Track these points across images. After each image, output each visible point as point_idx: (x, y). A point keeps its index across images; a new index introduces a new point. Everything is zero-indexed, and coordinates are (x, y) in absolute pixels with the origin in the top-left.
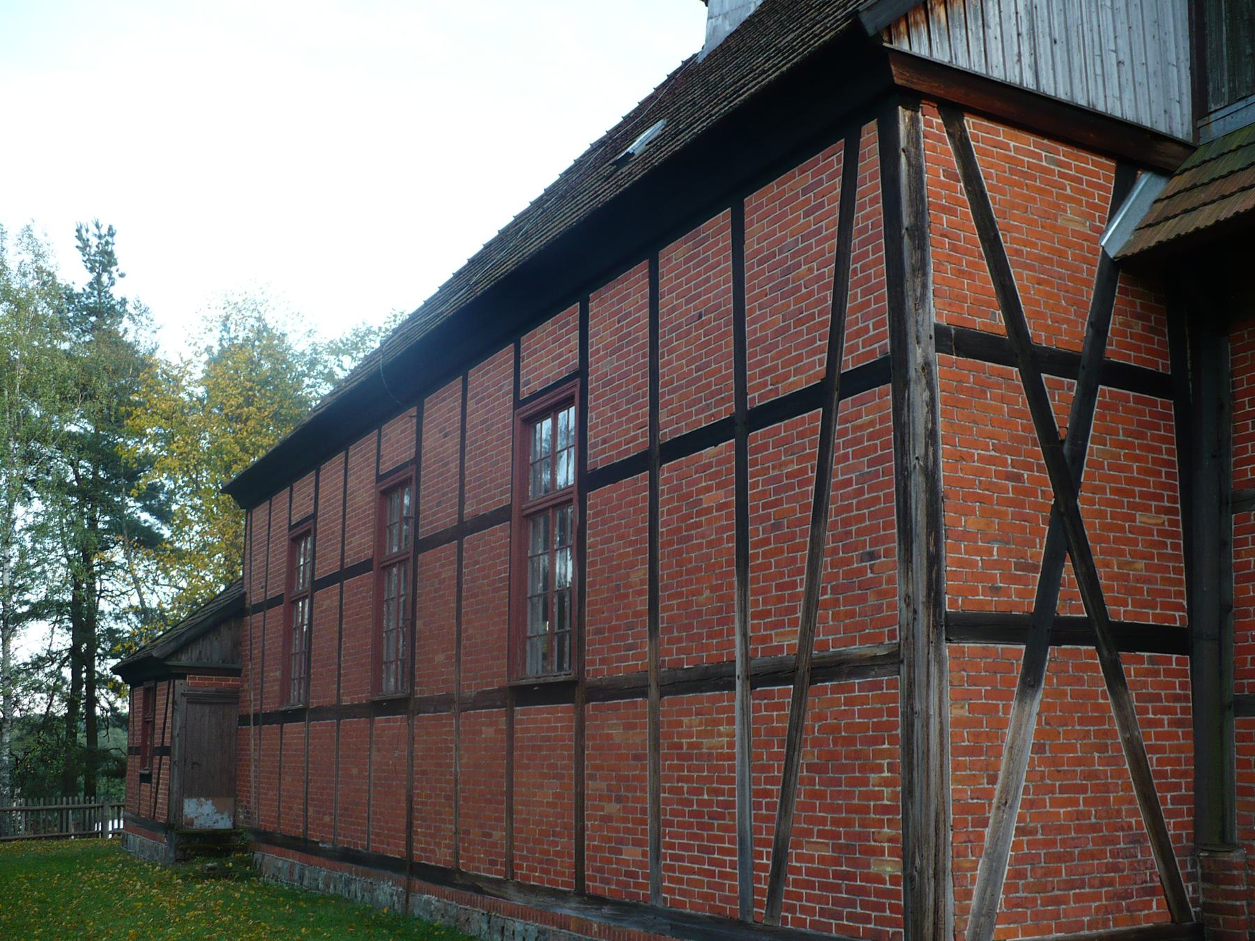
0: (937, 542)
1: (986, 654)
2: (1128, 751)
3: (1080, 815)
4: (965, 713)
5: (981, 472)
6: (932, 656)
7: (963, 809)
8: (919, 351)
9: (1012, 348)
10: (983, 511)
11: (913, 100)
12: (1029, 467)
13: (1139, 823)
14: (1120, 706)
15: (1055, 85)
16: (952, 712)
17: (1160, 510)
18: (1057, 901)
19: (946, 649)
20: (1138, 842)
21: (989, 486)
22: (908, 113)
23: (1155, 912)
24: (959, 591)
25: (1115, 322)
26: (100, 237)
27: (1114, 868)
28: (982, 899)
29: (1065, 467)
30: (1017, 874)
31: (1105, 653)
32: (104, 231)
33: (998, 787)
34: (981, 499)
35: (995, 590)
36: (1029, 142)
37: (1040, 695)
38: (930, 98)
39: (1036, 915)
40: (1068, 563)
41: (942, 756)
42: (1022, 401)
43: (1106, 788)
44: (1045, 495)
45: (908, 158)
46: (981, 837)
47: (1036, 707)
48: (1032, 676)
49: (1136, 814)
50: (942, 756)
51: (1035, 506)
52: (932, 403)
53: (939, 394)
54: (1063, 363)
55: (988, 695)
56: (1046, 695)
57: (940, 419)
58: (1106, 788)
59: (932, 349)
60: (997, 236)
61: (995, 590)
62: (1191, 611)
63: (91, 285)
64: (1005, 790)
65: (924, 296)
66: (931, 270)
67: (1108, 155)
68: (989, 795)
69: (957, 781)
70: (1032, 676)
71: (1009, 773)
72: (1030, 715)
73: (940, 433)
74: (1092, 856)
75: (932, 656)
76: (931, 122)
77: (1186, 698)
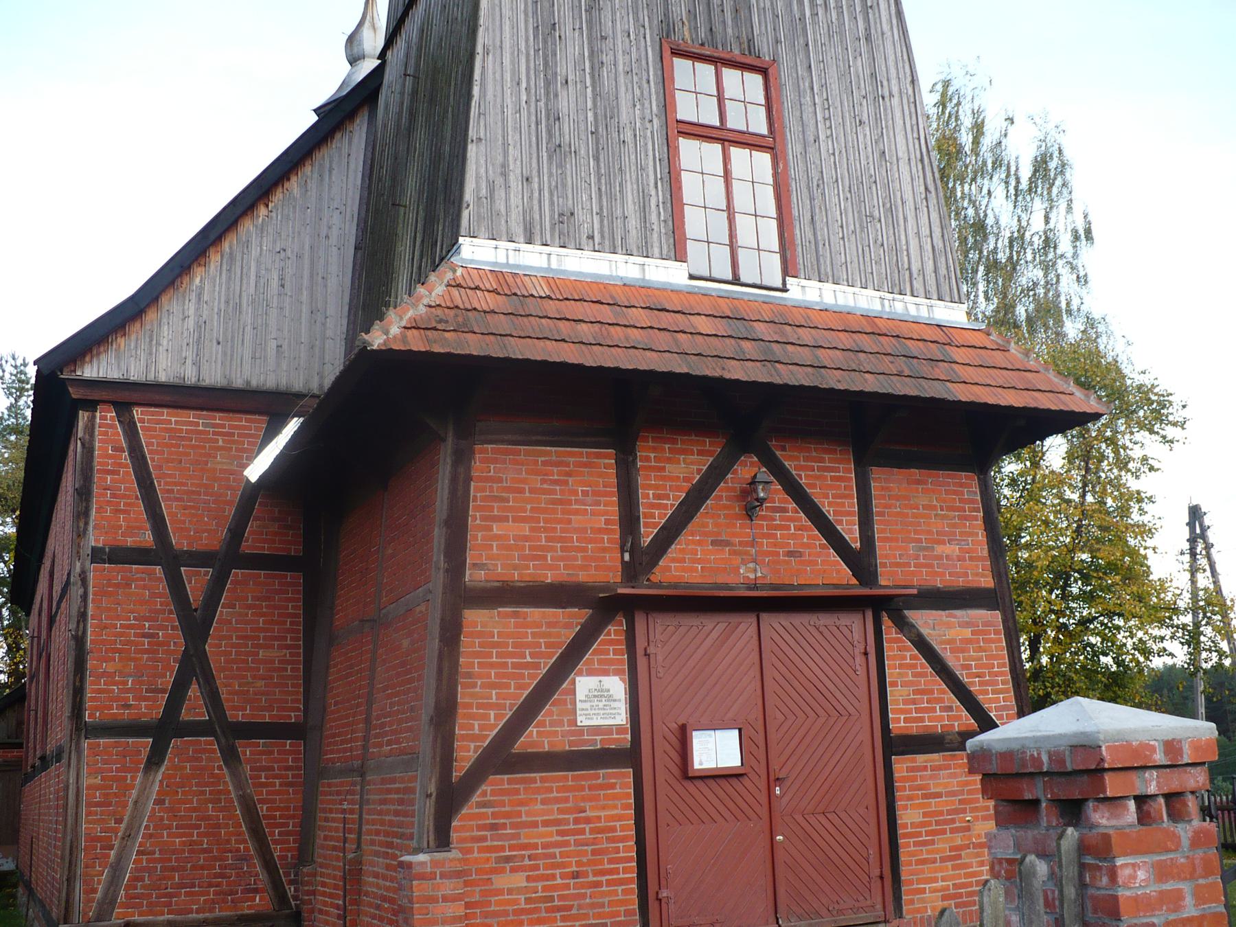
0: (82, 680)
1: (117, 745)
2: (240, 803)
3: (191, 843)
4: (98, 781)
5: (121, 634)
6: (73, 748)
7: (93, 839)
8: (78, 564)
9: (163, 554)
10: (121, 659)
11: (91, 405)
12: (164, 628)
13: (247, 849)
14: (235, 774)
15: (213, 376)
16: (86, 782)
17: (281, 647)
18: (170, 896)
19: (85, 744)
20: (245, 859)
21: (128, 643)
22: (86, 414)
23: (260, 902)
24: (97, 708)
25: (252, 526)
26: (16, 367)
27: (222, 876)
28: (106, 894)
29: (196, 625)
30: (135, 879)
31: (223, 741)
32: (19, 362)
33: (123, 826)
34: (119, 651)
35: (127, 706)
36: (191, 416)
37: (163, 769)
38: (104, 402)
39: (150, 904)
40: (194, 686)
41: (77, 807)
42: (163, 587)
43: (218, 826)
44: (178, 643)
45: (83, 444)
46: (108, 856)
47: (159, 777)
48: (155, 760)
49: (245, 841)
50: (77, 807)
51: (167, 652)
52: (85, 597)
53: (91, 590)
54: (199, 559)
55: (118, 770)
56: (167, 769)
57: (91, 605)
58: (218, 826)
59: (88, 562)
60: (152, 483)
61: (127, 706)
62: (306, 710)
63: (9, 409)
64: (130, 827)
65: (85, 530)
66: (93, 513)
67: (261, 413)
68: (115, 831)
69: (88, 822)
70: (155, 760)
71: (133, 818)
72: (153, 781)
73: (90, 613)
74: (202, 868)
75: (73, 748)
76: (106, 417)
77: (299, 768)
